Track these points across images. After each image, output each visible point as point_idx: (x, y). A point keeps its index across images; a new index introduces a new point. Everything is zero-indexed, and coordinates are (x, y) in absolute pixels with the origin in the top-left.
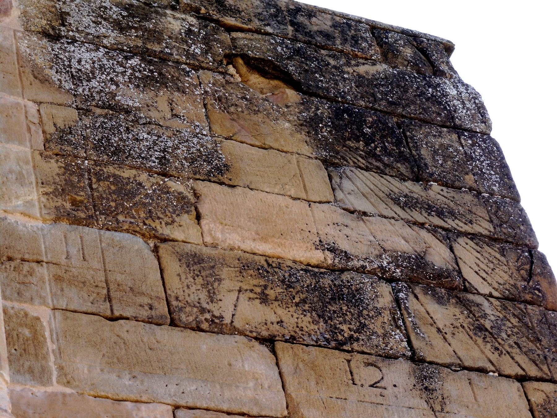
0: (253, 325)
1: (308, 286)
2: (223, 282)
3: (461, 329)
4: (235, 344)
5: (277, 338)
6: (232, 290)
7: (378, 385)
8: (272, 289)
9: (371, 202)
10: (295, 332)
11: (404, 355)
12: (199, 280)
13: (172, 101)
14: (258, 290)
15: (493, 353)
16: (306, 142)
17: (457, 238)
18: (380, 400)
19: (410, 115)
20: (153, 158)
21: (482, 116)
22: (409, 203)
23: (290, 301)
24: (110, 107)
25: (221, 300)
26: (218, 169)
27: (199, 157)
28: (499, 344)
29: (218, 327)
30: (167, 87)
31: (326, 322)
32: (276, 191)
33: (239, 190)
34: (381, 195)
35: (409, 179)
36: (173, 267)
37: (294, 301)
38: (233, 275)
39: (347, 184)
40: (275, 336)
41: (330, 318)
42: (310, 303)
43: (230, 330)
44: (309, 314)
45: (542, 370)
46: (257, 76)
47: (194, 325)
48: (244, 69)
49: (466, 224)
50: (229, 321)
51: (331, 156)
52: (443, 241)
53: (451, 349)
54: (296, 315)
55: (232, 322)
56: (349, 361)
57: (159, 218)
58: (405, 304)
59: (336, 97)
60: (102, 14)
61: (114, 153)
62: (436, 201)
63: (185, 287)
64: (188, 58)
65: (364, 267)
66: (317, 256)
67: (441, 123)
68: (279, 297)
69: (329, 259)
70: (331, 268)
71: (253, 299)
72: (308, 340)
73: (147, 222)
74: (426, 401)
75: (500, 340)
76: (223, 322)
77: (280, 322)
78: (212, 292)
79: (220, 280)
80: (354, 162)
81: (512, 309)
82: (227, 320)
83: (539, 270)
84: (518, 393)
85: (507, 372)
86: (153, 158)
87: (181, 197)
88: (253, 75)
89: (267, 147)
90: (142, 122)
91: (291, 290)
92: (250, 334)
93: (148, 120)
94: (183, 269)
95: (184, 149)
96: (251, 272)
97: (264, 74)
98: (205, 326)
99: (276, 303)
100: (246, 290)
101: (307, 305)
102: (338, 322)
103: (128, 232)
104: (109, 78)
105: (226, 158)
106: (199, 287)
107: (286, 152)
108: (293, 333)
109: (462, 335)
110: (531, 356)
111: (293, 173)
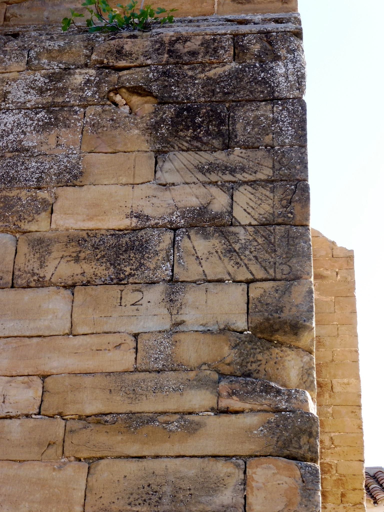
0: (64, 278)
1: (110, 246)
2: (52, 254)
3: (215, 254)
4: (48, 293)
5: (77, 284)
6: (57, 258)
7: (137, 303)
8: (84, 252)
9: (181, 175)
10: (91, 278)
11: (164, 280)
12: (37, 255)
13: (60, 135)
14: (75, 255)
15: (233, 267)
16: (147, 141)
17: (239, 187)
18: (135, 313)
19: (238, 99)
20: (34, 179)
21: (299, 85)
22: (213, 168)
23: (93, 258)
24: (17, 150)
25: (47, 266)
26: (75, 177)
27: (65, 170)
28: (241, 259)
29: (41, 283)
30: (58, 127)
31: (115, 267)
32: (112, 182)
33: (85, 187)
34: (191, 167)
35: (219, 149)
36: (24, 248)
37: (96, 258)
38: (60, 248)
39: (168, 165)
40: (76, 283)
41: (119, 264)
42: (108, 257)
43: (49, 284)
44: (105, 264)
45: (268, 273)
46: (136, 97)
47: (25, 285)
48: (126, 95)
49: (251, 174)
50: (49, 278)
51: (163, 147)
52: (227, 192)
53: (201, 269)
54: (95, 267)
55: (51, 278)
56: (122, 291)
57: (24, 219)
58: (178, 243)
59: (183, 100)
60: (32, 85)
61: (9, 182)
62: (233, 163)
63: (27, 261)
64: (80, 101)
65: (157, 224)
66: (125, 223)
67: (263, 99)
68: (87, 257)
69: (134, 222)
70: (135, 229)
71: (70, 261)
72: (98, 282)
73: (16, 223)
74: (168, 309)
75: (242, 257)
76: (45, 280)
77: (83, 274)
78: (43, 262)
79: (50, 253)
80: (179, 147)
81: (262, 232)
82: (47, 278)
83: (297, 198)
84: (242, 292)
85: (239, 278)
86: (34, 179)
87: (44, 201)
88: (134, 97)
89: (117, 151)
90: (35, 155)
91: (96, 250)
92: (60, 285)
93: (39, 153)
94: (29, 250)
95: (56, 167)
96: (73, 244)
97: (140, 95)
98: (33, 284)
99: (84, 261)
100: (67, 256)
101: (105, 259)
102: (123, 266)
103: (3, 232)
104: (21, 131)
105: (83, 167)
106: (36, 260)
107: (129, 152)
108: (89, 279)
109: (214, 259)
110: (264, 264)
111: (128, 166)
